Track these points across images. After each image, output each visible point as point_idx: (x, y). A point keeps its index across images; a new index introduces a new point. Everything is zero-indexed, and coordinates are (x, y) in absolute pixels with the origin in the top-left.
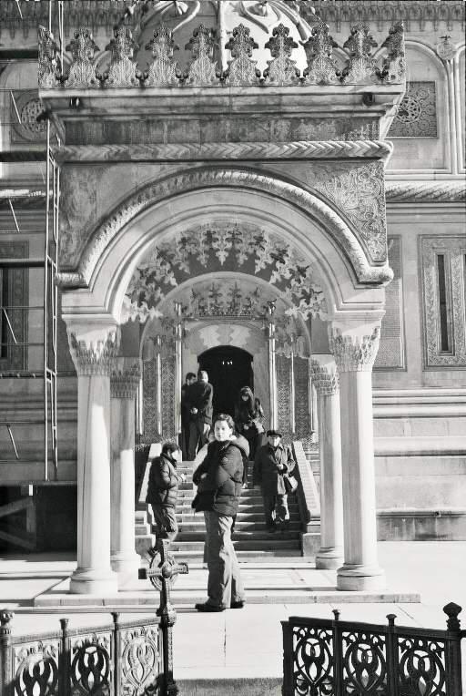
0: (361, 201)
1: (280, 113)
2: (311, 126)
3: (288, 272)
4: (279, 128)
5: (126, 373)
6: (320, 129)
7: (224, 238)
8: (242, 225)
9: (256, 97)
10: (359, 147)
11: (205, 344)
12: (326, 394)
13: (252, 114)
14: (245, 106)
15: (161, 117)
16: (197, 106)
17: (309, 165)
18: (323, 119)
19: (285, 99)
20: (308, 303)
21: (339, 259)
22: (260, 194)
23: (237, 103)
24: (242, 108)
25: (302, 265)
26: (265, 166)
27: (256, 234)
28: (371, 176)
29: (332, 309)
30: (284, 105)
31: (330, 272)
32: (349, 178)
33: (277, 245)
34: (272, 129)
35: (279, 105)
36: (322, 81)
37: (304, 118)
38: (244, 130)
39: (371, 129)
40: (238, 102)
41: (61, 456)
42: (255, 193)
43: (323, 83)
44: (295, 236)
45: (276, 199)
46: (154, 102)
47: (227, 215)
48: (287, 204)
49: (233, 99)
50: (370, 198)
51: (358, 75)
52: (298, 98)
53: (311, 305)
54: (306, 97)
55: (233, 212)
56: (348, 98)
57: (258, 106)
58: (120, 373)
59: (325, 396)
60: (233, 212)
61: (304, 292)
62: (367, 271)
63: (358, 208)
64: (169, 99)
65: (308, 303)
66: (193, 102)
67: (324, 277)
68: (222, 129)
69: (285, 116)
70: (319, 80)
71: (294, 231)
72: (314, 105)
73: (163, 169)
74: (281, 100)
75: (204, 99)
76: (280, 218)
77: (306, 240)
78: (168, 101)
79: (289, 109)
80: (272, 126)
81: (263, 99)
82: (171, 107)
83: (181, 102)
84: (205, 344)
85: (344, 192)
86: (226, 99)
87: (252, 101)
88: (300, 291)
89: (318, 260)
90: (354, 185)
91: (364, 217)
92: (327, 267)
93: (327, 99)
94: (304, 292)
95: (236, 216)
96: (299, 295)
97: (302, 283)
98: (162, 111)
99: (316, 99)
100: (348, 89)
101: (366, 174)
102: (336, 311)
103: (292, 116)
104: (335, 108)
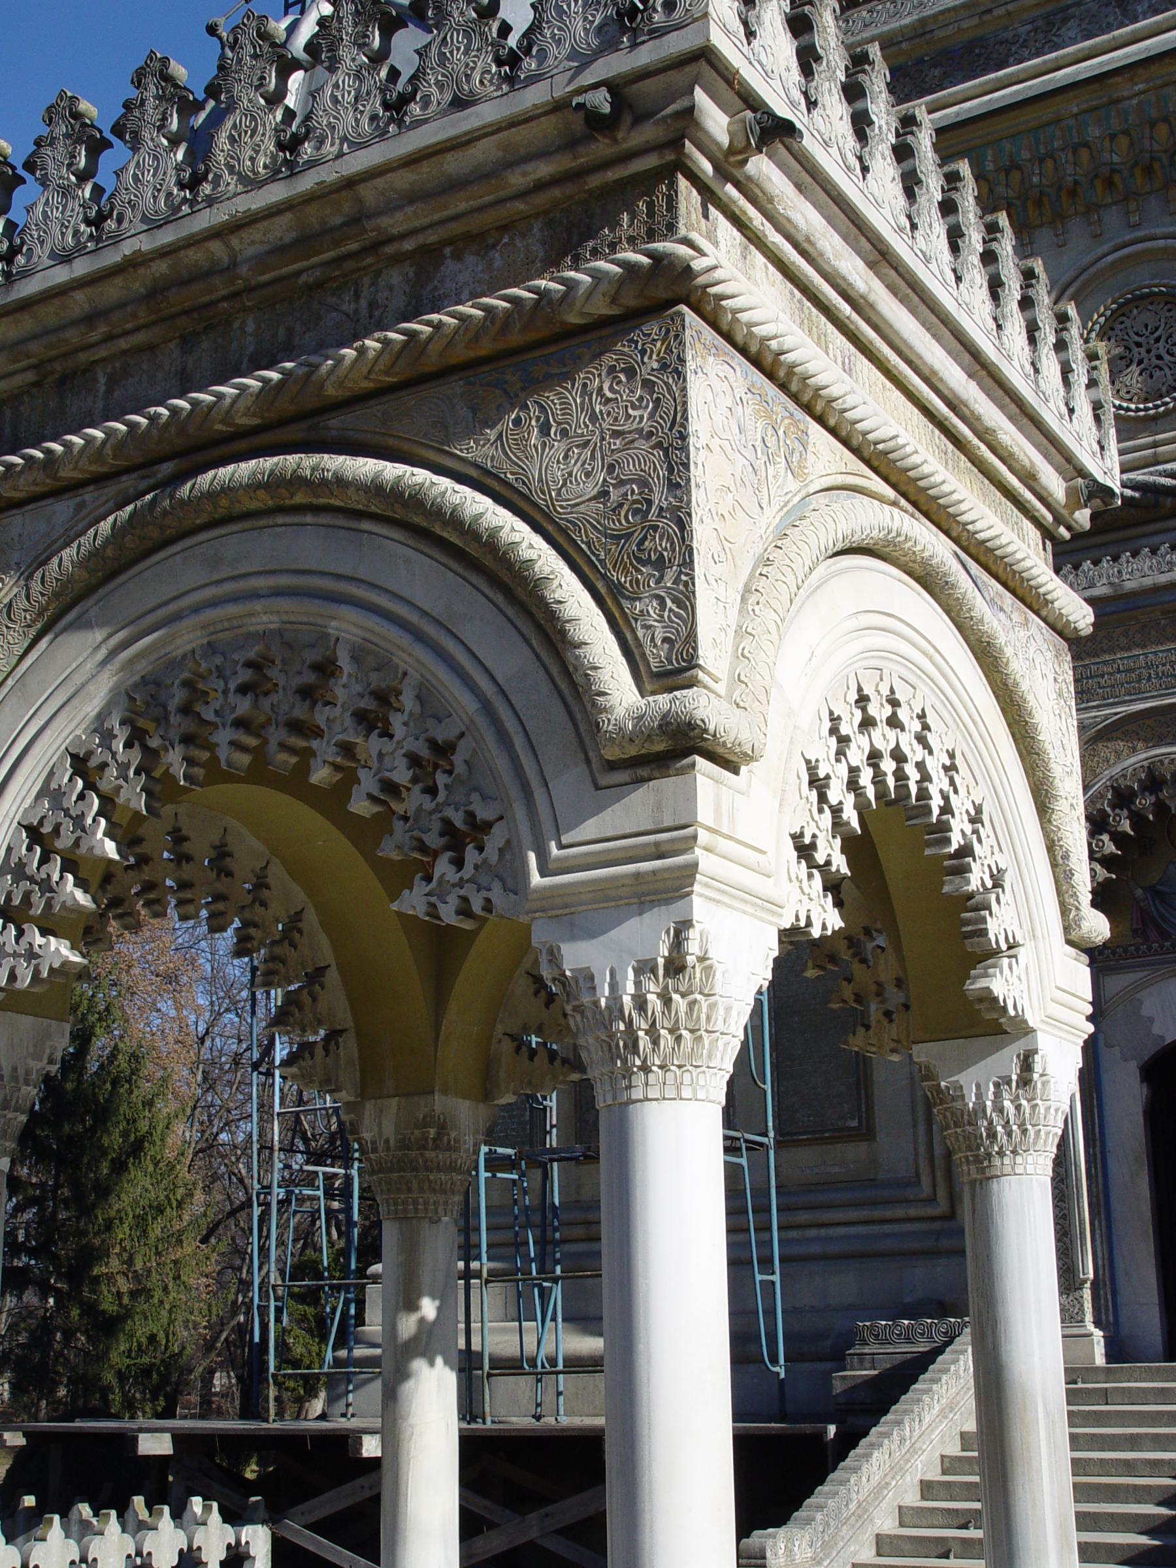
0: (611, 468)
1: (374, 247)
2: (470, 259)
3: (401, 763)
4: (382, 297)
5: (404, 1144)
6: (498, 263)
7: (232, 686)
8: (280, 633)
9: (287, 218)
10: (588, 279)
11: (1156, 1030)
12: (974, 1176)
13: (299, 273)
14: (268, 253)
15: (83, 357)
16: (155, 293)
17: (456, 386)
18: (504, 228)
19: (369, 193)
20: (459, 863)
21: (545, 687)
22: (324, 519)
23: (251, 251)
24: (261, 262)
25: (442, 734)
26: (335, 423)
27: (312, 656)
28: (644, 372)
29: (526, 875)
30: (379, 213)
31: (519, 742)
32: (575, 398)
33: (374, 677)
34: (363, 303)
35: (356, 221)
36: (455, 98)
37: (449, 242)
38: (290, 332)
39: (651, 213)
40: (249, 245)
41: (868, 1365)
42: (309, 519)
43: (460, 103)
44: (420, 637)
45: (366, 525)
46: (49, 314)
47: (232, 609)
48: (396, 534)
49: (235, 241)
50: (643, 444)
51: (559, 42)
52: (403, 180)
53: (468, 871)
54: (425, 168)
55: (255, 595)
56: (549, 126)
57: (305, 243)
58: (387, 1141)
59: (973, 1183)
60: (255, 595)
61: (448, 828)
62: (620, 712)
63: (604, 494)
64: (79, 296)
65: (459, 863)
66: (138, 284)
67: (501, 763)
68: (234, 345)
69: (390, 249)
70: (448, 97)
71: (413, 617)
72: (454, 185)
73: (80, 506)
74: (360, 201)
75: (161, 267)
76: (373, 586)
77: (450, 645)
78: (80, 301)
79: (395, 223)
80: (365, 293)
81: (313, 214)
82: (90, 319)
83: (112, 291)
84: (1156, 1030)
85: (559, 447)
86: (216, 247)
87: (281, 229)
88: (437, 826)
89: (487, 708)
90: (594, 418)
91: (624, 521)
92: (510, 724)
93: (484, 152)
94: (448, 828)
95: (258, 606)
96: (433, 840)
97: (442, 796)
98: (73, 336)
99: (454, 164)
100: (534, 96)
101: (631, 372)
102: (536, 879)
103: (408, 245)
104: (517, 180)
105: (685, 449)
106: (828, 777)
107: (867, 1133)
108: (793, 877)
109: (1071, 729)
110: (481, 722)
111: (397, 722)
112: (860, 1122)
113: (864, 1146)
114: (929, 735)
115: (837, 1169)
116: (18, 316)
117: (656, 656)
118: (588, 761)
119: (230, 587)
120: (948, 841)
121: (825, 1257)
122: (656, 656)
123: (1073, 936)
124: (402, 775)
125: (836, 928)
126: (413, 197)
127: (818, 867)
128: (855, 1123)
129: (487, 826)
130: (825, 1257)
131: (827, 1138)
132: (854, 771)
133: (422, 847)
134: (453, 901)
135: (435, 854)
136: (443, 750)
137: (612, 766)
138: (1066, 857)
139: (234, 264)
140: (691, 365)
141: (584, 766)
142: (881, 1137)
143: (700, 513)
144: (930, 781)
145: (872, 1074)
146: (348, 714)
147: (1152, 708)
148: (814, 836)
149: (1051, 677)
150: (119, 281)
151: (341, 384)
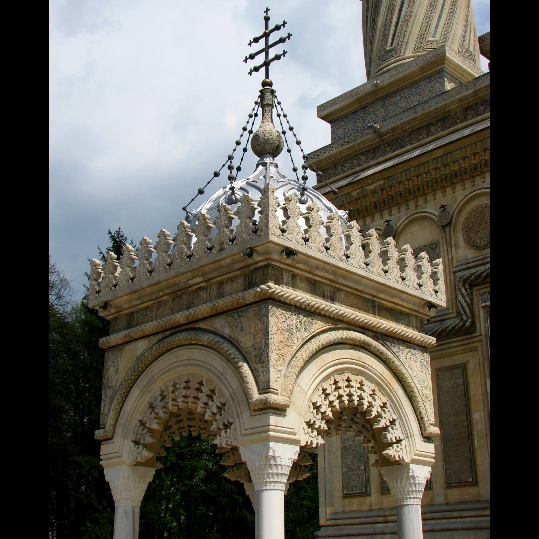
23: (183, 281)
54: (217, 264)
86: (175, 279)
88: (222, 423)
105: (268, 335)
106: (321, 405)
107: (475, 483)
108: (306, 432)
109: (428, 375)
110: (230, 399)
111: (214, 397)
112: (473, 479)
113: (475, 488)
114: (363, 387)
115: (466, 497)
116: (135, 293)
117: (262, 385)
118: (250, 410)
119: (181, 363)
120: (371, 415)
121: (463, 529)
122: (262, 385)
123: (425, 435)
124: (215, 411)
125: (322, 443)
126: (215, 270)
127: (316, 429)
128: (471, 480)
129: (231, 424)
130: (463, 529)
131: (462, 485)
132: (331, 403)
133: (219, 428)
134: (225, 442)
135: (222, 430)
136: (224, 405)
137: (255, 411)
138: (420, 413)
139: (180, 283)
140: (270, 314)
141: (249, 410)
142: (481, 485)
143: (272, 350)
144: (364, 399)
145: (476, 463)
146: (205, 395)
147: (388, 391)
148: (314, 421)
149: (418, 361)
150: (156, 286)
151: (202, 315)
